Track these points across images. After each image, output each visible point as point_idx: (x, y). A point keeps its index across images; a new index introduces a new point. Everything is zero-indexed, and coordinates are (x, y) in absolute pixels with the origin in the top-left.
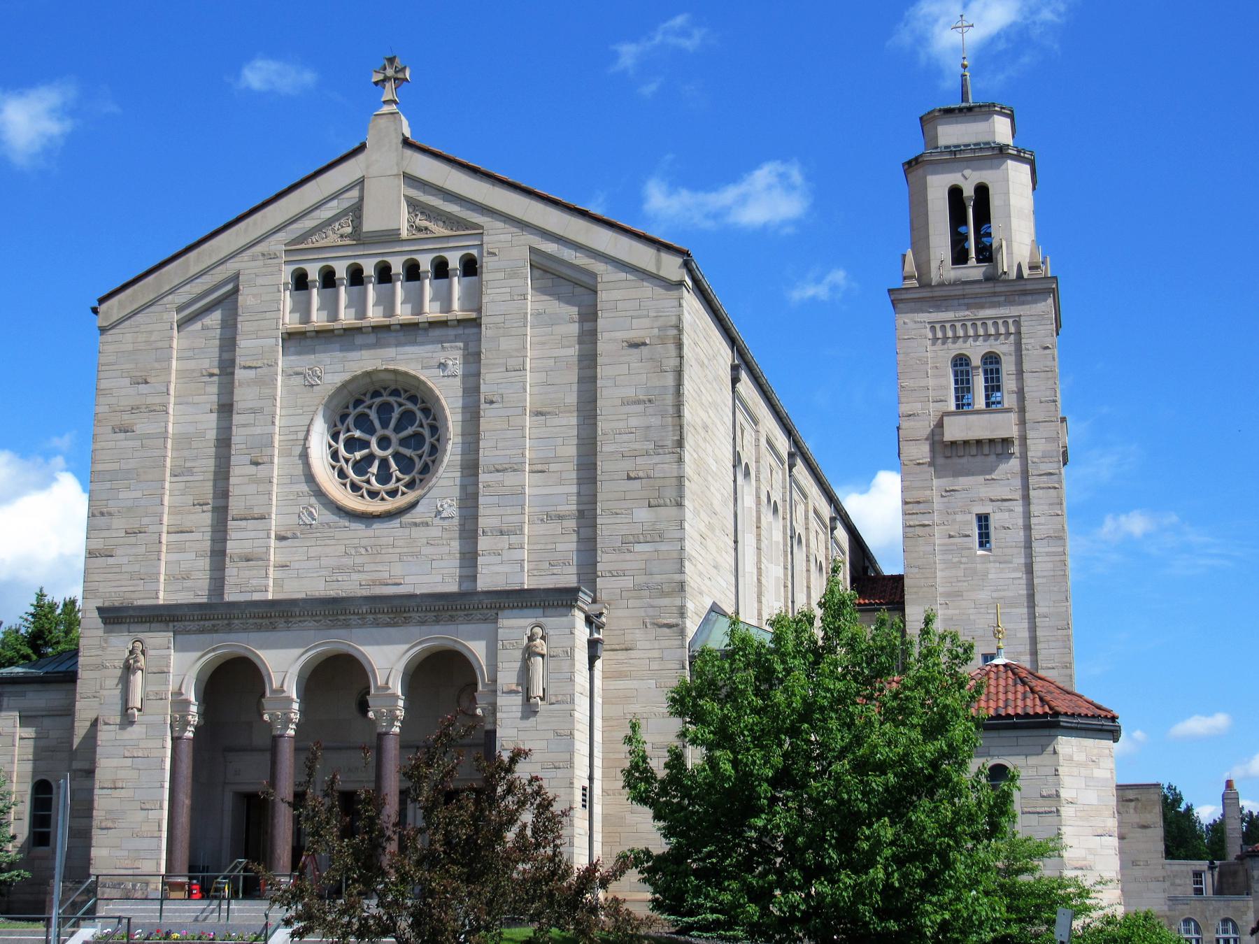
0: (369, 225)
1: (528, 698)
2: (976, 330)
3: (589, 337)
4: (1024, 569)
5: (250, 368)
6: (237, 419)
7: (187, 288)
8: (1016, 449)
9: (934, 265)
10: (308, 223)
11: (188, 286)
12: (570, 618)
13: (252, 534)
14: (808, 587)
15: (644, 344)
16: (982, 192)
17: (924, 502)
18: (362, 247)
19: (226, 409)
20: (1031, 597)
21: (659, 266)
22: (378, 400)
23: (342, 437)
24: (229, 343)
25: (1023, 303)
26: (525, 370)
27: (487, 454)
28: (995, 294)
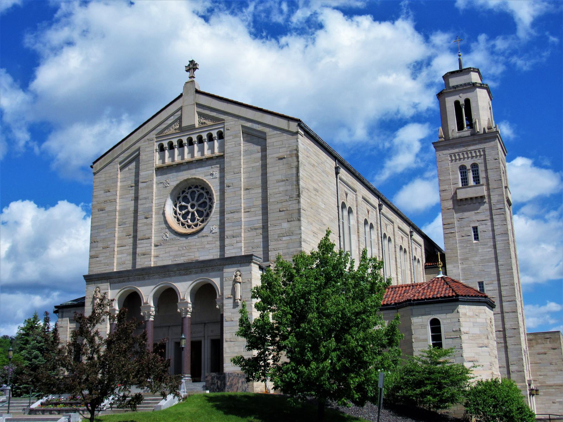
0: (184, 125)
1: (235, 300)
2: (468, 155)
3: (264, 158)
4: (493, 247)
5: (144, 182)
6: (140, 202)
7: (122, 155)
8: (486, 200)
9: (450, 132)
10: (163, 126)
11: (123, 154)
12: (250, 267)
13: (146, 245)
14: (396, 258)
15: (284, 158)
16: (467, 101)
17: (451, 224)
18: (182, 133)
19: (136, 199)
20: (496, 258)
21: (289, 126)
22: (190, 190)
23: (178, 205)
24: (137, 174)
25: (486, 143)
26: (241, 173)
27: (227, 207)
28: (474, 140)
